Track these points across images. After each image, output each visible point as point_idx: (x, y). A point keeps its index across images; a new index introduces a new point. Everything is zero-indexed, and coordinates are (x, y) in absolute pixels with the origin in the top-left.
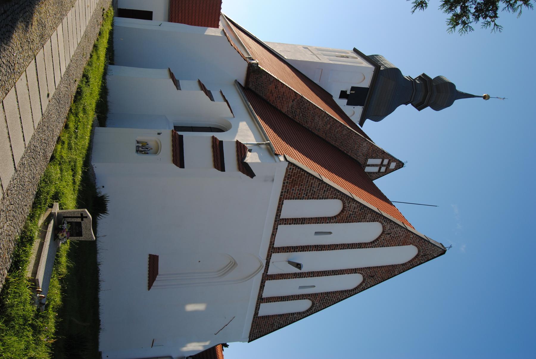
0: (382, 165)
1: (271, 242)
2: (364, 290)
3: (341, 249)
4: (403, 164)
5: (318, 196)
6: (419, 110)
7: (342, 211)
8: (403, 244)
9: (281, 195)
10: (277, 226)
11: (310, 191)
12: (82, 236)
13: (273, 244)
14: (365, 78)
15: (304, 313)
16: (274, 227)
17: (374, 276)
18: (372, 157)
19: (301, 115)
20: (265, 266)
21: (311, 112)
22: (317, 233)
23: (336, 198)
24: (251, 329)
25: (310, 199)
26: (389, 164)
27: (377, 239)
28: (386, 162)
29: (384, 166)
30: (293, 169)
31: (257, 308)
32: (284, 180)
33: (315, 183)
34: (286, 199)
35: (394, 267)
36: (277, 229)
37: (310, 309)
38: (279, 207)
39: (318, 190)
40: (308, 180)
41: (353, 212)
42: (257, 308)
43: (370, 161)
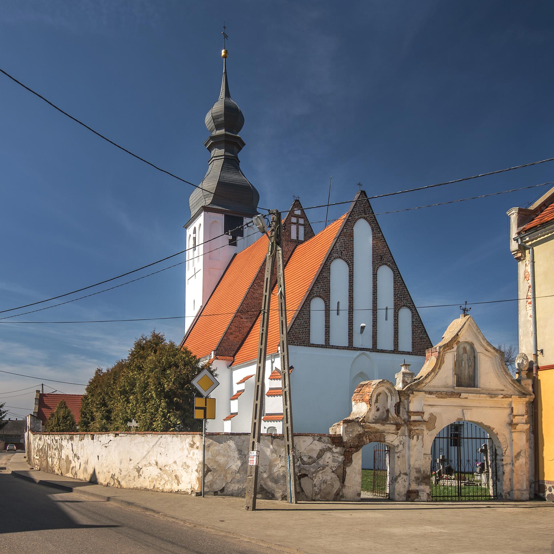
0: (297, 224)
1: (343, 349)
7: (320, 297)
8: (352, 236)
16: (331, 348)
18: (290, 235)
19: (253, 310)
21: (250, 301)
28: (294, 220)
29: (298, 221)
32: (295, 345)
38: (315, 347)
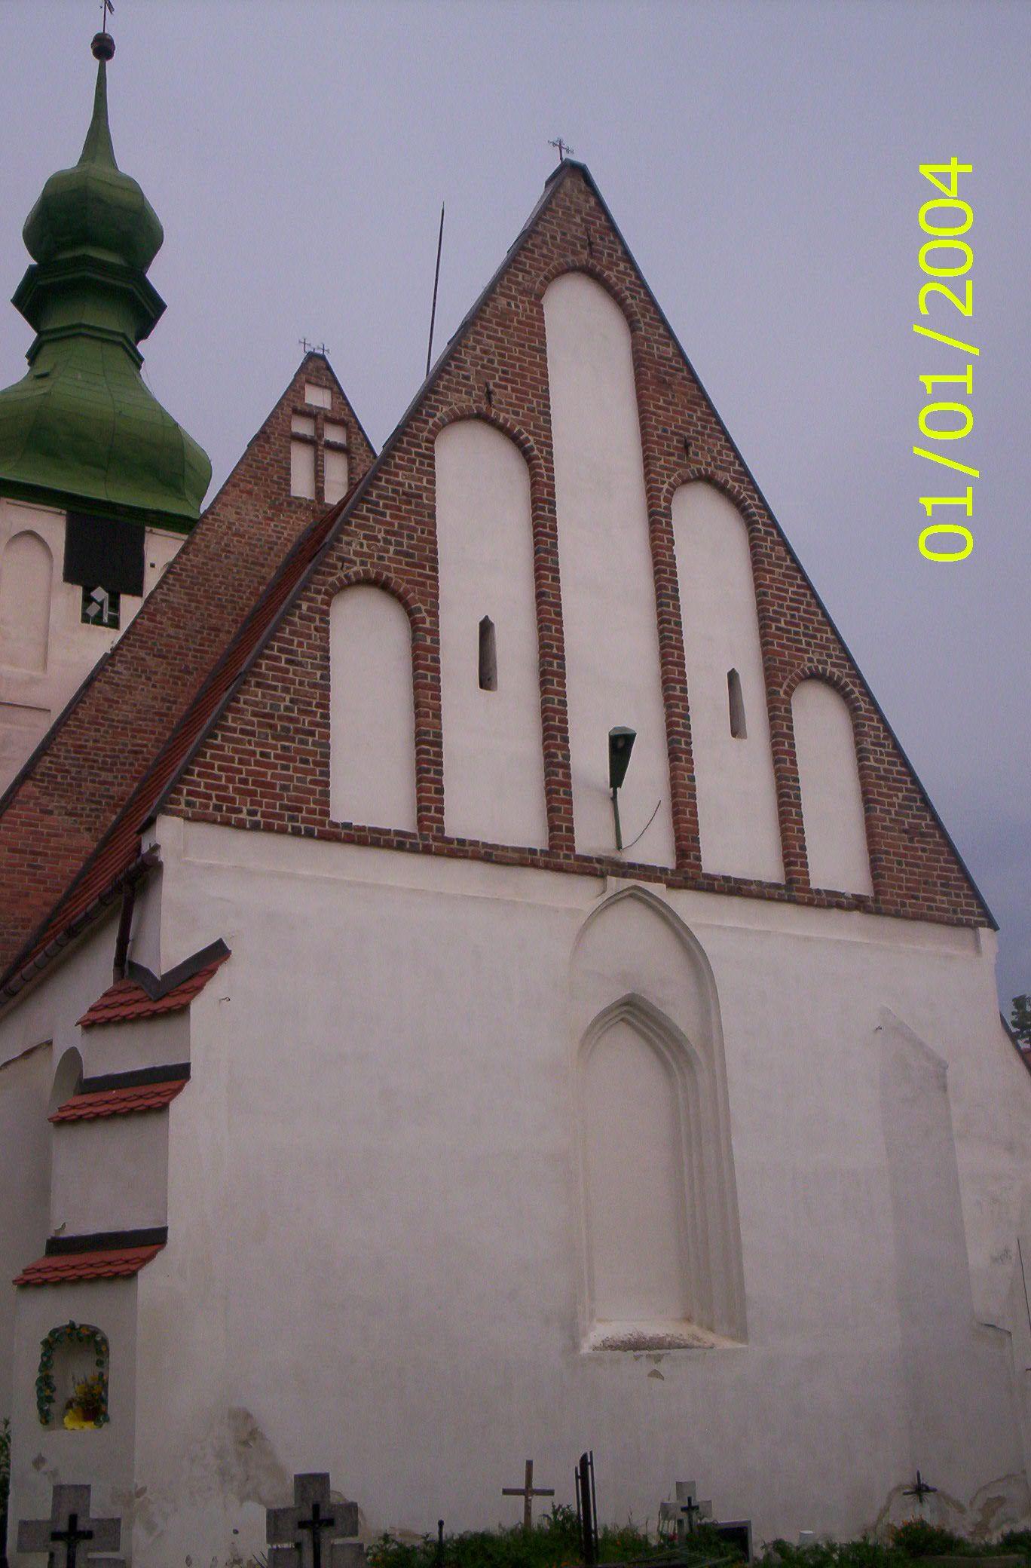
2: (747, 473)
3: (556, 579)
4: (311, 357)
5: (314, 685)
6: (160, 307)
7: (382, 585)
9: (309, 834)
10: (450, 841)
11: (291, 720)
12: (117, 1549)
13: (533, 851)
14: (31, 534)
15: (853, 710)
17: (682, 435)
19: (104, 775)
20: (632, 882)
22: (486, 680)
23: (326, 613)
24: (932, 920)
25: (326, 716)
26: (310, 414)
27: (514, 439)
28: (302, 427)
30: (190, 793)
31: (832, 901)
32: (240, 826)
33: (256, 704)
34: (327, 814)
35: (640, 361)
36: (461, 842)
37: (833, 684)
39: (286, 690)
40: (243, 732)
41: (387, 542)
42: (832, 901)
43: (301, 486)
